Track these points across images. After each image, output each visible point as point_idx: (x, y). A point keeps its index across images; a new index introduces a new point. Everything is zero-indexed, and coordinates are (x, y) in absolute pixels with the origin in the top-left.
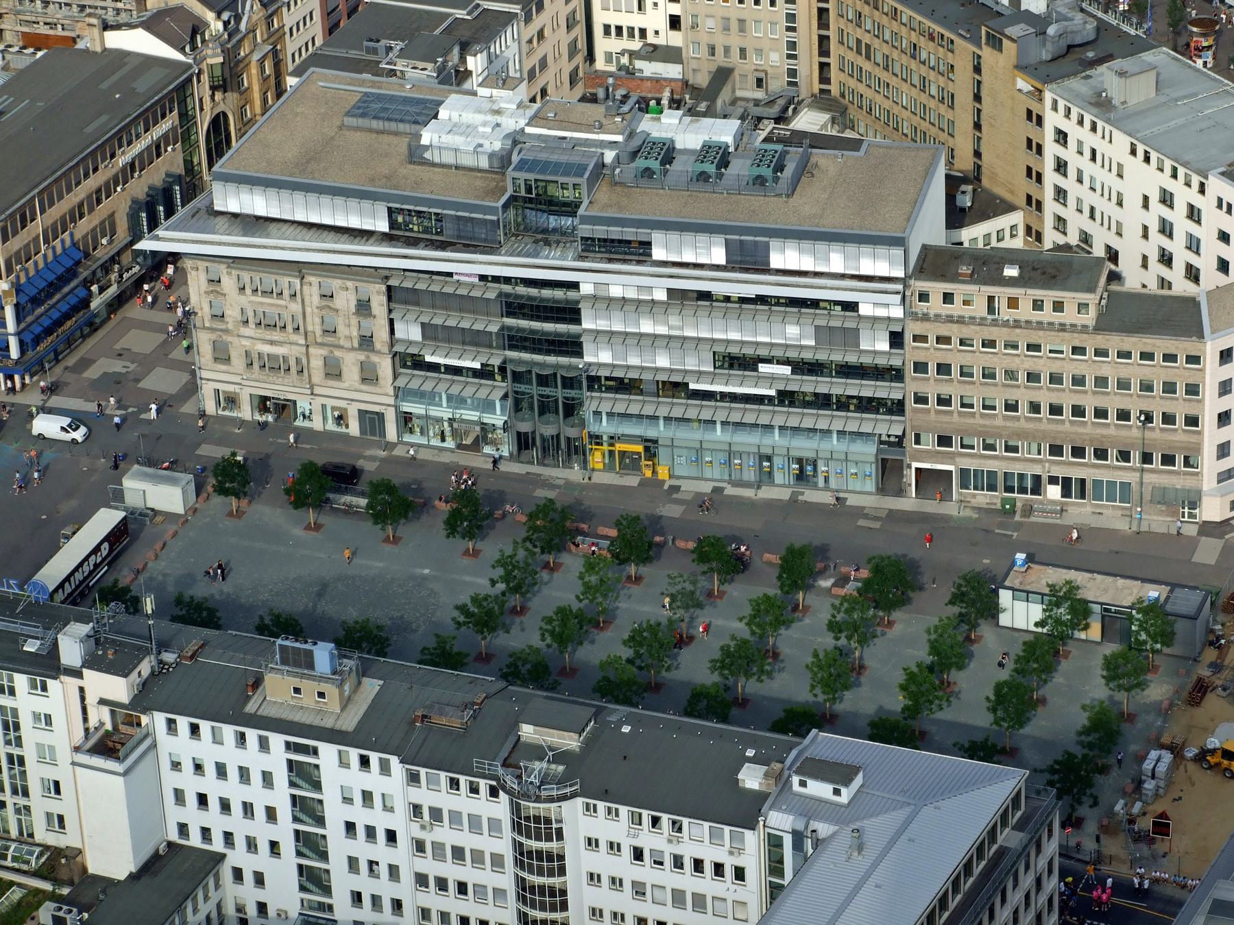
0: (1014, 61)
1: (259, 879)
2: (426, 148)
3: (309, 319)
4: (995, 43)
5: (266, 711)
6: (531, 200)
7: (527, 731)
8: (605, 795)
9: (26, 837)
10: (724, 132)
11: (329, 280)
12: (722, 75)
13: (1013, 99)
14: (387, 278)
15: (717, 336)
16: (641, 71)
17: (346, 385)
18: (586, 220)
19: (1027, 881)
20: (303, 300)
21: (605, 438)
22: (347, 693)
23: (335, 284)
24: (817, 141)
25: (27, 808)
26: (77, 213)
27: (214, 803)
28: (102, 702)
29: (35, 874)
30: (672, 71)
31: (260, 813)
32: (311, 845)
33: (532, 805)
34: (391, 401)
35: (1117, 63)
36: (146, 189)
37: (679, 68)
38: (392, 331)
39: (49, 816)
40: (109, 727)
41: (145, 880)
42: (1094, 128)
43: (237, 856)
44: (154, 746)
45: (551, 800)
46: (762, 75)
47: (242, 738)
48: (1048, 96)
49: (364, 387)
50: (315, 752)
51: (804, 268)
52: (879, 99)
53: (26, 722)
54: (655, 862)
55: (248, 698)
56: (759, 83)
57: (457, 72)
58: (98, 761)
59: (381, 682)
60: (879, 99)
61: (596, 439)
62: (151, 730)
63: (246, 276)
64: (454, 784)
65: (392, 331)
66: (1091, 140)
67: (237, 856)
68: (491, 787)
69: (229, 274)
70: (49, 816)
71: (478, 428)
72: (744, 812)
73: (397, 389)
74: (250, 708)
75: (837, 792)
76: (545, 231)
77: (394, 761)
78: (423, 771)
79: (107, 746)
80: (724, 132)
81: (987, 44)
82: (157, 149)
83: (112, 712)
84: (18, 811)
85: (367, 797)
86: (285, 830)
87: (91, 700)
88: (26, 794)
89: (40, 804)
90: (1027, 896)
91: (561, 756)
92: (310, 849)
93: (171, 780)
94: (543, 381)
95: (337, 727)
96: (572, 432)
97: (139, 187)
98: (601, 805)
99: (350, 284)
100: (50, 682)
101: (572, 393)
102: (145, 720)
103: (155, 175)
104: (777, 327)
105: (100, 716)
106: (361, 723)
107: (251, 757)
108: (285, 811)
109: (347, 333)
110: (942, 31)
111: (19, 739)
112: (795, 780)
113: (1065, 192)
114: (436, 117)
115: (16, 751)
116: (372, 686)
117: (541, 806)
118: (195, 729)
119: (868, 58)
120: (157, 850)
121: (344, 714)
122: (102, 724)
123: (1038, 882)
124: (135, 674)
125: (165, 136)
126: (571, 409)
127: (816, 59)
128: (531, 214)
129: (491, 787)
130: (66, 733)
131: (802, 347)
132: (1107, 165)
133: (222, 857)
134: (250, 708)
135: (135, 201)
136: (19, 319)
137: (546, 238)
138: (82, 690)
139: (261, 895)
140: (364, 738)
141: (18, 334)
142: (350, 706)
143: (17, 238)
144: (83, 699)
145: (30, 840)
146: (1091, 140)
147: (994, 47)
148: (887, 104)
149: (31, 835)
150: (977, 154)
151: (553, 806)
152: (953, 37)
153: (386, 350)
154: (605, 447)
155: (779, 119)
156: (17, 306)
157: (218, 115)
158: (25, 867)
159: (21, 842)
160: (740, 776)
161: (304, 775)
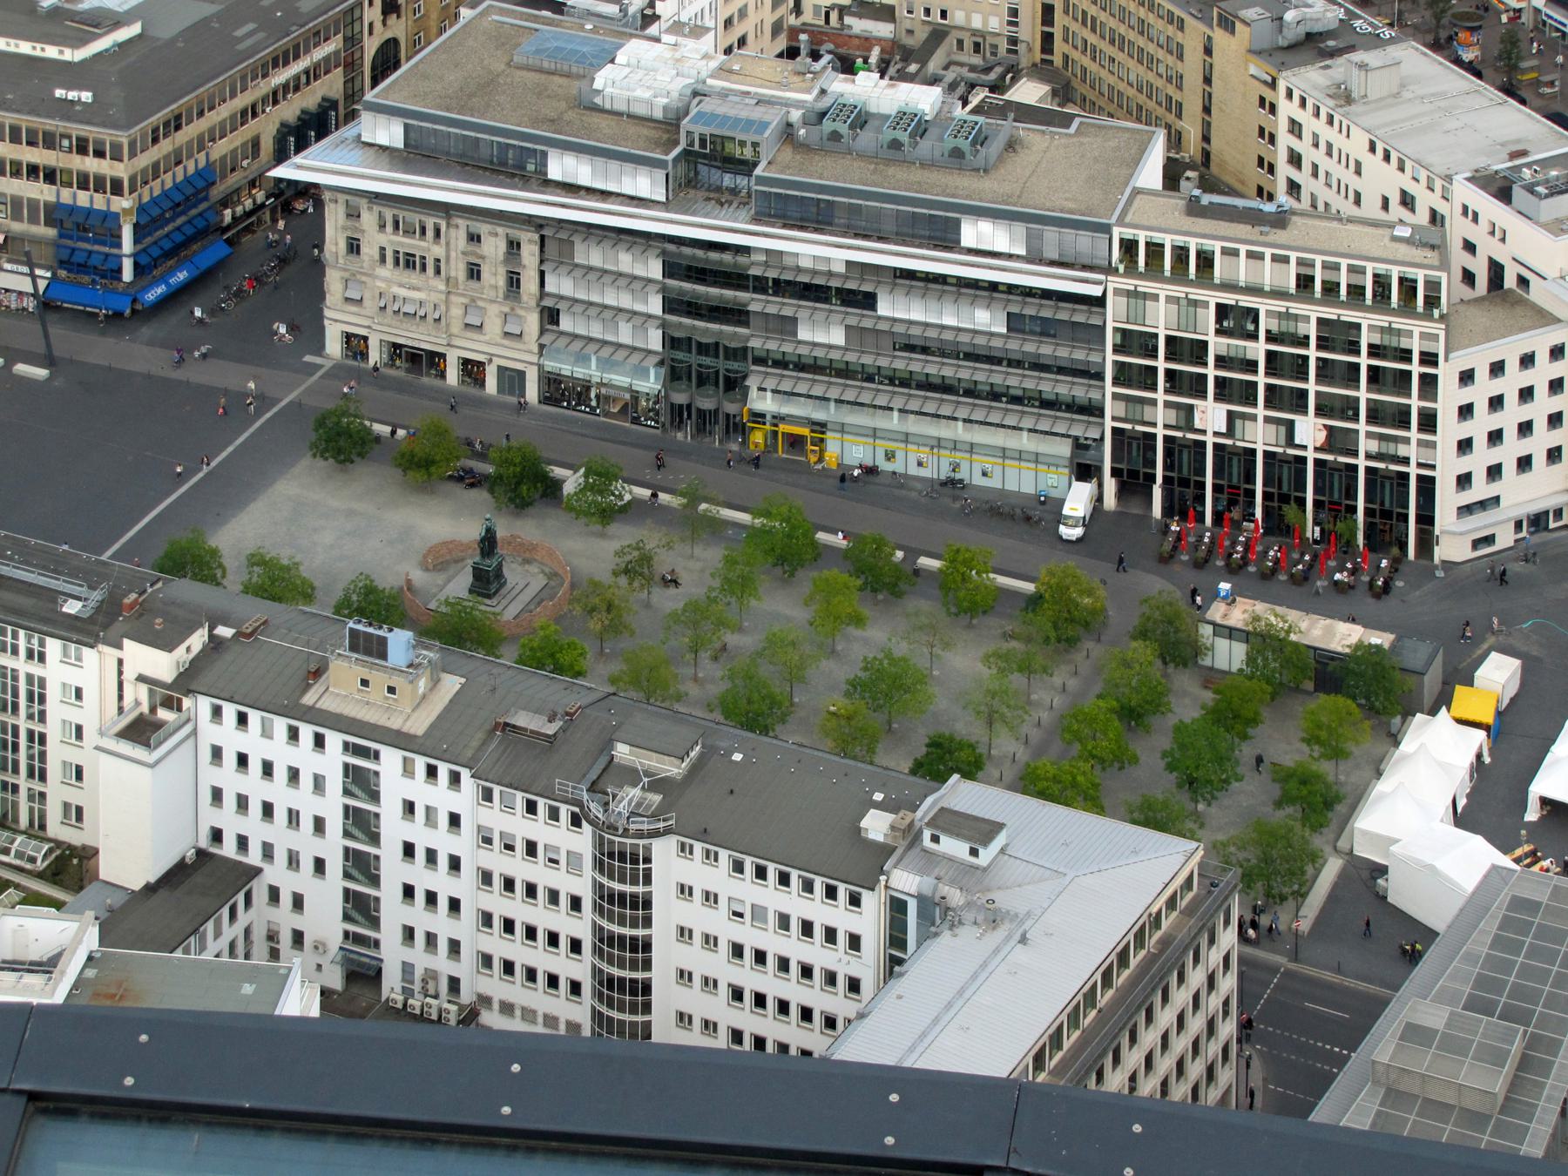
0: (1246, 44)
1: (298, 902)
2: (598, 92)
3: (453, 262)
4: (1228, 24)
5: (328, 704)
6: (704, 156)
7: (622, 751)
8: (703, 835)
9: (38, 828)
10: (924, 99)
11: (478, 225)
12: (938, 36)
13: (1245, 84)
14: (541, 226)
15: (898, 315)
16: (850, 27)
17: (487, 338)
18: (761, 180)
19: (1196, 978)
20: (448, 244)
21: (768, 417)
22: (421, 691)
23: (483, 228)
24: (1026, 113)
25: (42, 795)
26: (220, 132)
27: (280, 815)
28: (141, 679)
29: (40, 876)
30: (883, 30)
31: (307, 824)
32: (362, 866)
33: (617, 839)
34: (535, 359)
35: (1357, 56)
36: (298, 113)
37: (890, 27)
38: (542, 283)
39: (66, 806)
40: (145, 708)
41: (163, 893)
42: (1330, 121)
43: (275, 873)
44: (194, 732)
45: (640, 835)
46: (980, 40)
47: (294, 735)
48: (1282, 86)
49: (506, 342)
50: (377, 755)
51: (997, 249)
52: (1104, 74)
53: (53, 693)
54: (551, 860)
55: (308, 687)
56: (977, 48)
57: (644, 16)
58: (125, 747)
59: (463, 680)
60: (1104, 74)
61: (758, 417)
62: (192, 716)
63: (389, 214)
64: (531, 808)
65: (542, 283)
66: (1328, 134)
67: (275, 873)
68: (573, 814)
69: (370, 209)
70: (66, 806)
71: (627, 396)
72: (861, 867)
73: (542, 347)
74: (309, 699)
75: (974, 852)
76: (719, 189)
77: (465, 774)
78: (497, 790)
79: (141, 731)
80: (924, 99)
81: (1219, 25)
82: (312, 74)
83: (150, 691)
84: (31, 798)
85: (531, 848)
86: (333, 846)
87: (129, 674)
88: (43, 777)
89: (57, 791)
90: (1196, 998)
91: (658, 784)
92: (360, 871)
93: (211, 776)
94: (703, 349)
95: (405, 729)
96: (731, 408)
97: (289, 110)
98: (698, 847)
99: (500, 230)
100: (85, 650)
101: (735, 365)
102: (187, 703)
103: (309, 99)
104: (965, 309)
105: (138, 696)
106: (433, 726)
107: (303, 755)
108: (335, 824)
109: (493, 282)
110: (1172, 8)
111: (42, 714)
112: (927, 834)
113: (1299, 187)
114: (612, 61)
115: (38, 728)
116: (452, 684)
117: (628, 841)
118: (242, 719)
119: (1093, 30)
120: (183, 858)
121: (416, 714)
122: (138, 703)
123: (1211, 982)
124: (181, 649)
125: (327, 59)
126: (734, 385)
127: (1039, 28)
128: (703, 169)
129: (573, 814)
130: (97, 713)
131: (992, 334)
132: (1345, 160)
133: (258, 871)
134: (309, 699)
135: (283, 125)
136: (136, 241)
137: (723, 198)
138: (120, 662)
139: (298, 922)
140: (433, 748)
141: (134, 255)
142: (423, 706)
143: (146, 154)
144: (120, 673)
145: (41, 834)
146: (1328, 134)
147: (1226, 29)
148: (1112, 80)
149: (43, 827)
150: (1206, 139)
151: (641, 842)
152: (1183, 15)
153: (533, 303)
154: (768, 427)
155: (996, 88)
156: (136, 226)
157: (388, 41)
158: (29, 866)
159: (30, 836)
160: (863, 824)
161: (361, 782)
